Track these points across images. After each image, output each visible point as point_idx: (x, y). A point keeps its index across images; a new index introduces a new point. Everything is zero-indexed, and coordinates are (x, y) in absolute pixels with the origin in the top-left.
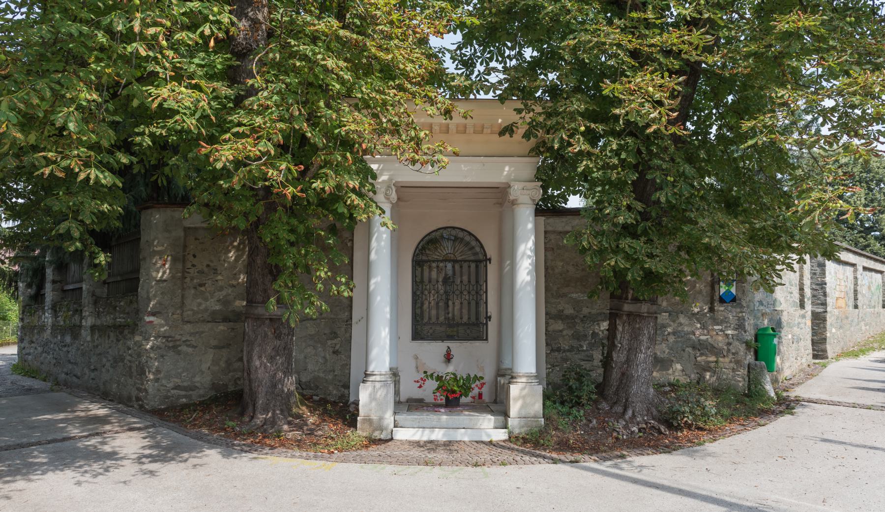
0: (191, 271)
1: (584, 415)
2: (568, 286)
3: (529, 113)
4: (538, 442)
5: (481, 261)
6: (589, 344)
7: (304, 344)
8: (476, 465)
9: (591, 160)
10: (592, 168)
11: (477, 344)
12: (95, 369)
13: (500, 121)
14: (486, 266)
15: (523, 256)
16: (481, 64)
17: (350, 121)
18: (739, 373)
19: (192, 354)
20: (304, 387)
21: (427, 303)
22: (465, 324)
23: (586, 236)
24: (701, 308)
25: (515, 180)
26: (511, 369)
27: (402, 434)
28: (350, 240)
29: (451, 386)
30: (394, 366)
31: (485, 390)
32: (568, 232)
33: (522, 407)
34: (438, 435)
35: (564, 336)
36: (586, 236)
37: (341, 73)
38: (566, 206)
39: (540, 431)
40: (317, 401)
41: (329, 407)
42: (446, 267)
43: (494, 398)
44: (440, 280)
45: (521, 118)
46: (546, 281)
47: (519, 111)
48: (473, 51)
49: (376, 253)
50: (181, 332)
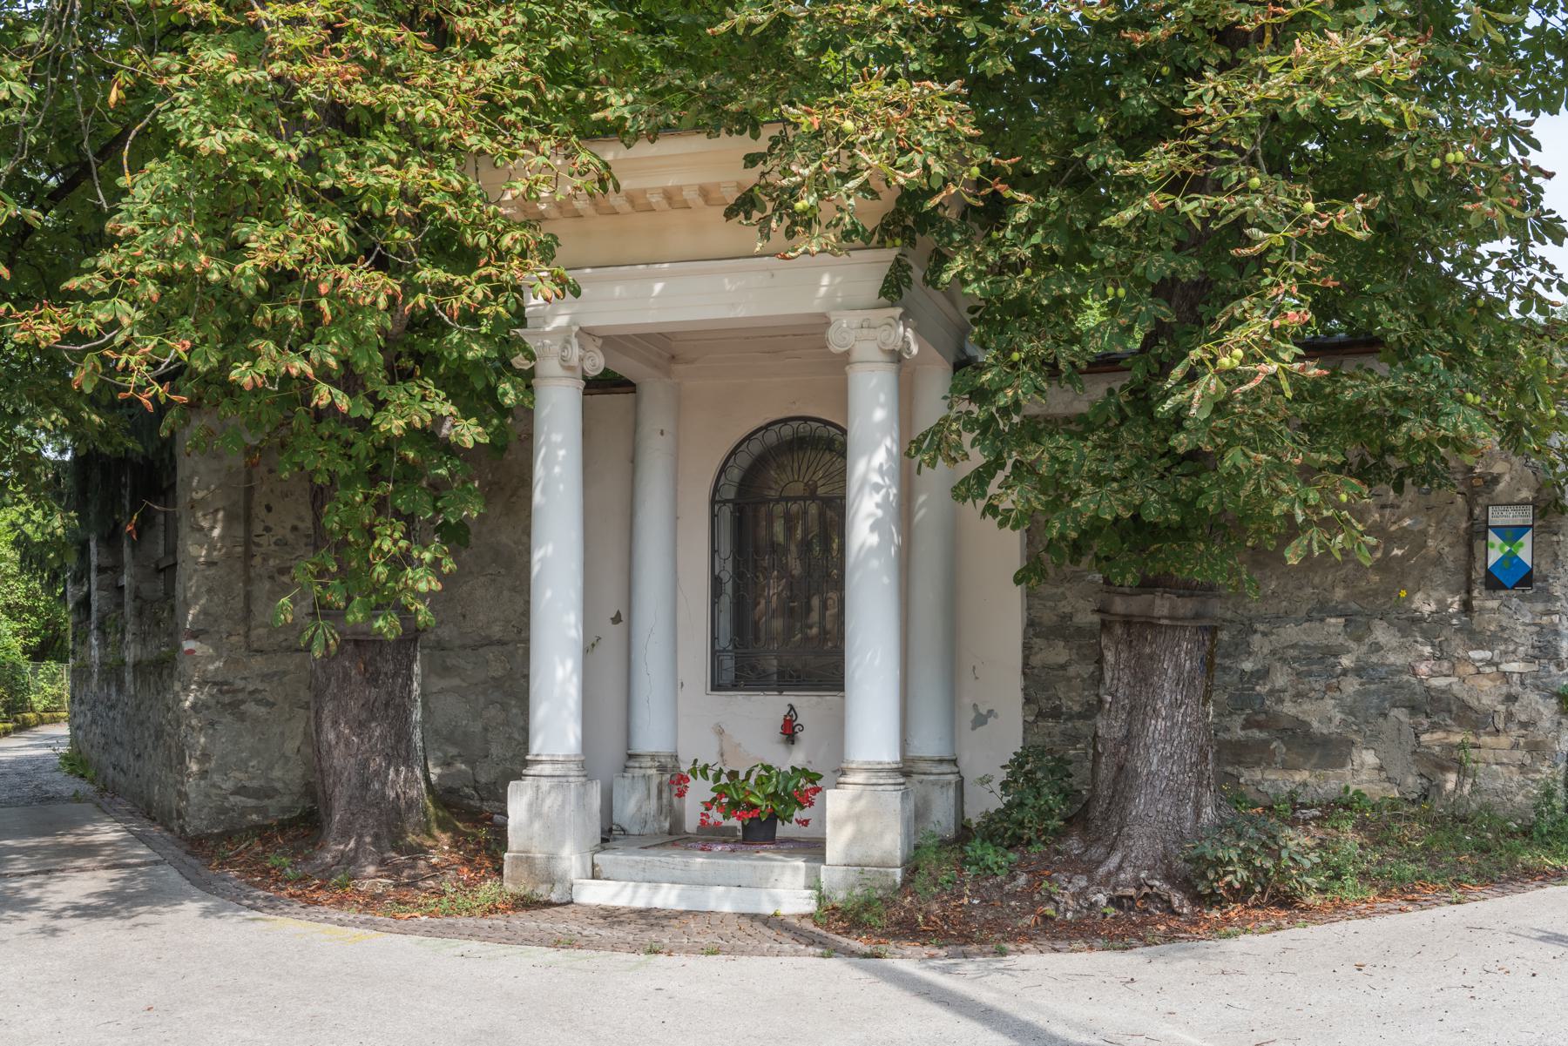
0: (263, 541)
7: (482, 699)
12: (139, 756)
15: (861, 489)
18: (1538, 776)
19: (267, 720)
20: (484, 794)
24: (1440, 602)
25: (837, 308)
27: (595, 894)
33: (853, 841)
34: (667, 897)
35: (1069, 679)
49: (543, 492)
50: (246, 674)
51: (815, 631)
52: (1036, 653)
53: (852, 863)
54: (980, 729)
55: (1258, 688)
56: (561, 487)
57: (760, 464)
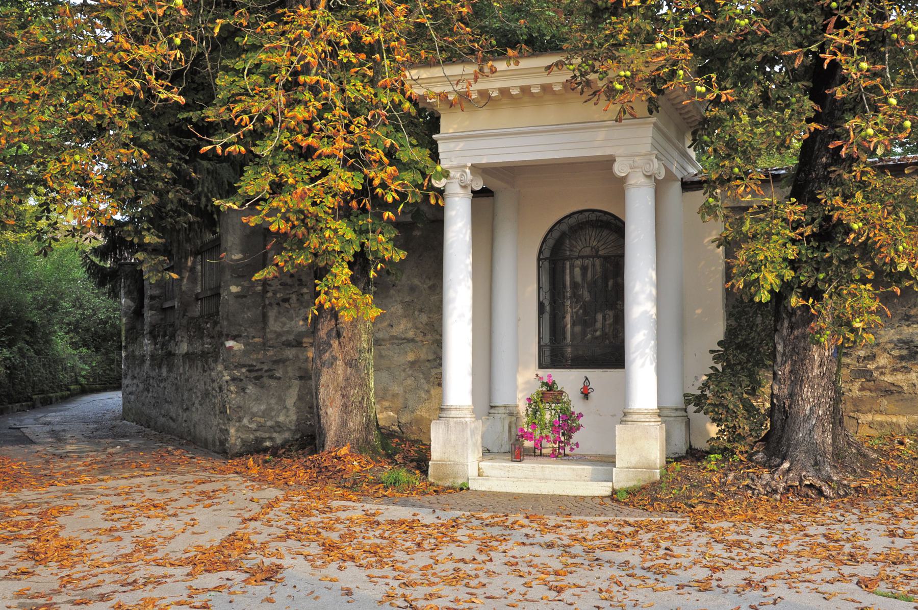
12: (187, 409)
51: (598, 333)
54: (592, 395)
55: (868, 366)
57: (563, 235)
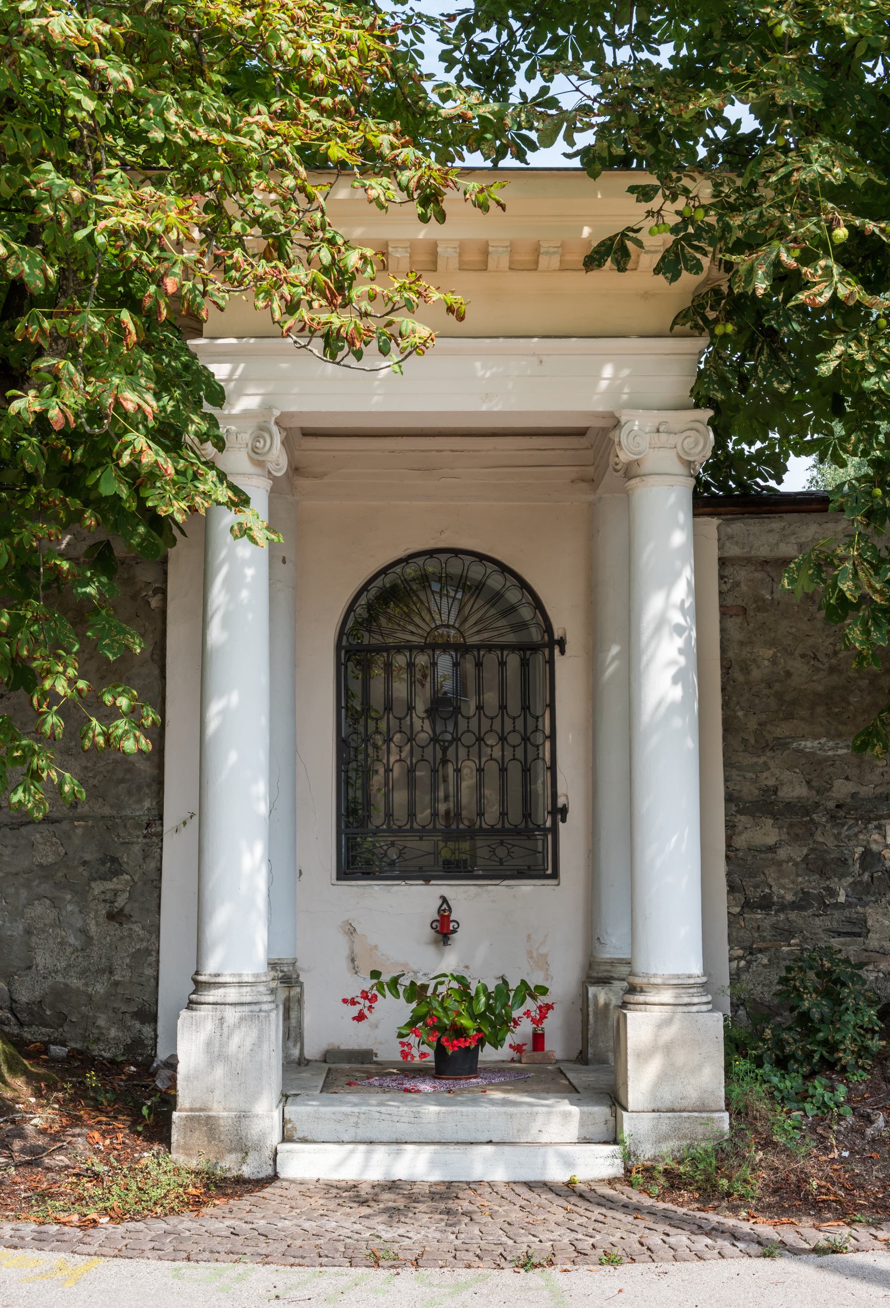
1: (849, 1100)
2: (789, 717)
3: (674, 199)
4: (714, 1186)
5: (534, 648)
6: (854, 884)
7: (24, 893)
8: (527, 1264)
9: (859, 340)
10: (863, 362)
11: (527, 888)
13: (586, 232)
14: (551, 662)
15: (658, 629)
16: (530, 75)
17: (124, 202)
20: (24, 1017)
21: (382, 771)
22: (492, 831)
23: (848, 565)
26: (628, 963)
28: (156, 591)
29: (452, 1015)
30: (284, 954)
31: (552, 1025)
32: (784, 562)
33: (663, 1078)
35: (780, 864)
36: (848, 565)
37: (99, 63)
38: (783, 488)
39: (720, 1152)
40: (61, 1060)
41: (92, 1078)
42: (434, 664)
43: (579, 1046)
44: (421, 706)
45: (650, 213)
46: (725, 705)
47: (644, 193)
48: (504, 37)
49: (226, 624)
52: (740, 833)
53: (662, 1106)
56: (250, 617)
